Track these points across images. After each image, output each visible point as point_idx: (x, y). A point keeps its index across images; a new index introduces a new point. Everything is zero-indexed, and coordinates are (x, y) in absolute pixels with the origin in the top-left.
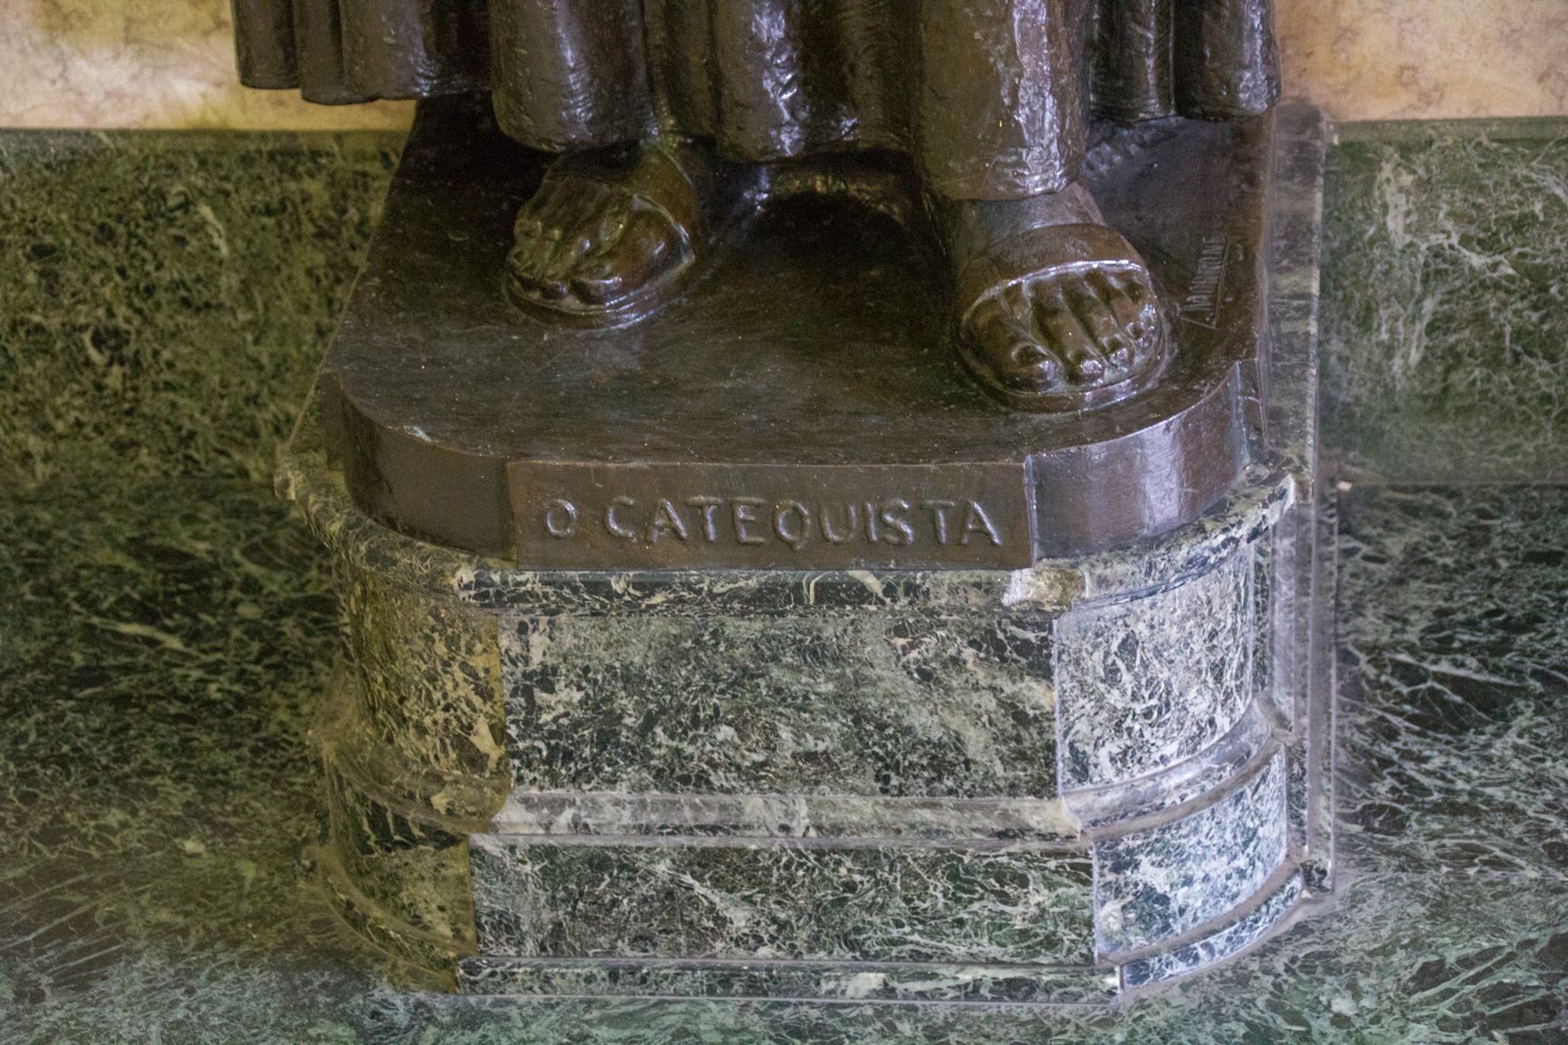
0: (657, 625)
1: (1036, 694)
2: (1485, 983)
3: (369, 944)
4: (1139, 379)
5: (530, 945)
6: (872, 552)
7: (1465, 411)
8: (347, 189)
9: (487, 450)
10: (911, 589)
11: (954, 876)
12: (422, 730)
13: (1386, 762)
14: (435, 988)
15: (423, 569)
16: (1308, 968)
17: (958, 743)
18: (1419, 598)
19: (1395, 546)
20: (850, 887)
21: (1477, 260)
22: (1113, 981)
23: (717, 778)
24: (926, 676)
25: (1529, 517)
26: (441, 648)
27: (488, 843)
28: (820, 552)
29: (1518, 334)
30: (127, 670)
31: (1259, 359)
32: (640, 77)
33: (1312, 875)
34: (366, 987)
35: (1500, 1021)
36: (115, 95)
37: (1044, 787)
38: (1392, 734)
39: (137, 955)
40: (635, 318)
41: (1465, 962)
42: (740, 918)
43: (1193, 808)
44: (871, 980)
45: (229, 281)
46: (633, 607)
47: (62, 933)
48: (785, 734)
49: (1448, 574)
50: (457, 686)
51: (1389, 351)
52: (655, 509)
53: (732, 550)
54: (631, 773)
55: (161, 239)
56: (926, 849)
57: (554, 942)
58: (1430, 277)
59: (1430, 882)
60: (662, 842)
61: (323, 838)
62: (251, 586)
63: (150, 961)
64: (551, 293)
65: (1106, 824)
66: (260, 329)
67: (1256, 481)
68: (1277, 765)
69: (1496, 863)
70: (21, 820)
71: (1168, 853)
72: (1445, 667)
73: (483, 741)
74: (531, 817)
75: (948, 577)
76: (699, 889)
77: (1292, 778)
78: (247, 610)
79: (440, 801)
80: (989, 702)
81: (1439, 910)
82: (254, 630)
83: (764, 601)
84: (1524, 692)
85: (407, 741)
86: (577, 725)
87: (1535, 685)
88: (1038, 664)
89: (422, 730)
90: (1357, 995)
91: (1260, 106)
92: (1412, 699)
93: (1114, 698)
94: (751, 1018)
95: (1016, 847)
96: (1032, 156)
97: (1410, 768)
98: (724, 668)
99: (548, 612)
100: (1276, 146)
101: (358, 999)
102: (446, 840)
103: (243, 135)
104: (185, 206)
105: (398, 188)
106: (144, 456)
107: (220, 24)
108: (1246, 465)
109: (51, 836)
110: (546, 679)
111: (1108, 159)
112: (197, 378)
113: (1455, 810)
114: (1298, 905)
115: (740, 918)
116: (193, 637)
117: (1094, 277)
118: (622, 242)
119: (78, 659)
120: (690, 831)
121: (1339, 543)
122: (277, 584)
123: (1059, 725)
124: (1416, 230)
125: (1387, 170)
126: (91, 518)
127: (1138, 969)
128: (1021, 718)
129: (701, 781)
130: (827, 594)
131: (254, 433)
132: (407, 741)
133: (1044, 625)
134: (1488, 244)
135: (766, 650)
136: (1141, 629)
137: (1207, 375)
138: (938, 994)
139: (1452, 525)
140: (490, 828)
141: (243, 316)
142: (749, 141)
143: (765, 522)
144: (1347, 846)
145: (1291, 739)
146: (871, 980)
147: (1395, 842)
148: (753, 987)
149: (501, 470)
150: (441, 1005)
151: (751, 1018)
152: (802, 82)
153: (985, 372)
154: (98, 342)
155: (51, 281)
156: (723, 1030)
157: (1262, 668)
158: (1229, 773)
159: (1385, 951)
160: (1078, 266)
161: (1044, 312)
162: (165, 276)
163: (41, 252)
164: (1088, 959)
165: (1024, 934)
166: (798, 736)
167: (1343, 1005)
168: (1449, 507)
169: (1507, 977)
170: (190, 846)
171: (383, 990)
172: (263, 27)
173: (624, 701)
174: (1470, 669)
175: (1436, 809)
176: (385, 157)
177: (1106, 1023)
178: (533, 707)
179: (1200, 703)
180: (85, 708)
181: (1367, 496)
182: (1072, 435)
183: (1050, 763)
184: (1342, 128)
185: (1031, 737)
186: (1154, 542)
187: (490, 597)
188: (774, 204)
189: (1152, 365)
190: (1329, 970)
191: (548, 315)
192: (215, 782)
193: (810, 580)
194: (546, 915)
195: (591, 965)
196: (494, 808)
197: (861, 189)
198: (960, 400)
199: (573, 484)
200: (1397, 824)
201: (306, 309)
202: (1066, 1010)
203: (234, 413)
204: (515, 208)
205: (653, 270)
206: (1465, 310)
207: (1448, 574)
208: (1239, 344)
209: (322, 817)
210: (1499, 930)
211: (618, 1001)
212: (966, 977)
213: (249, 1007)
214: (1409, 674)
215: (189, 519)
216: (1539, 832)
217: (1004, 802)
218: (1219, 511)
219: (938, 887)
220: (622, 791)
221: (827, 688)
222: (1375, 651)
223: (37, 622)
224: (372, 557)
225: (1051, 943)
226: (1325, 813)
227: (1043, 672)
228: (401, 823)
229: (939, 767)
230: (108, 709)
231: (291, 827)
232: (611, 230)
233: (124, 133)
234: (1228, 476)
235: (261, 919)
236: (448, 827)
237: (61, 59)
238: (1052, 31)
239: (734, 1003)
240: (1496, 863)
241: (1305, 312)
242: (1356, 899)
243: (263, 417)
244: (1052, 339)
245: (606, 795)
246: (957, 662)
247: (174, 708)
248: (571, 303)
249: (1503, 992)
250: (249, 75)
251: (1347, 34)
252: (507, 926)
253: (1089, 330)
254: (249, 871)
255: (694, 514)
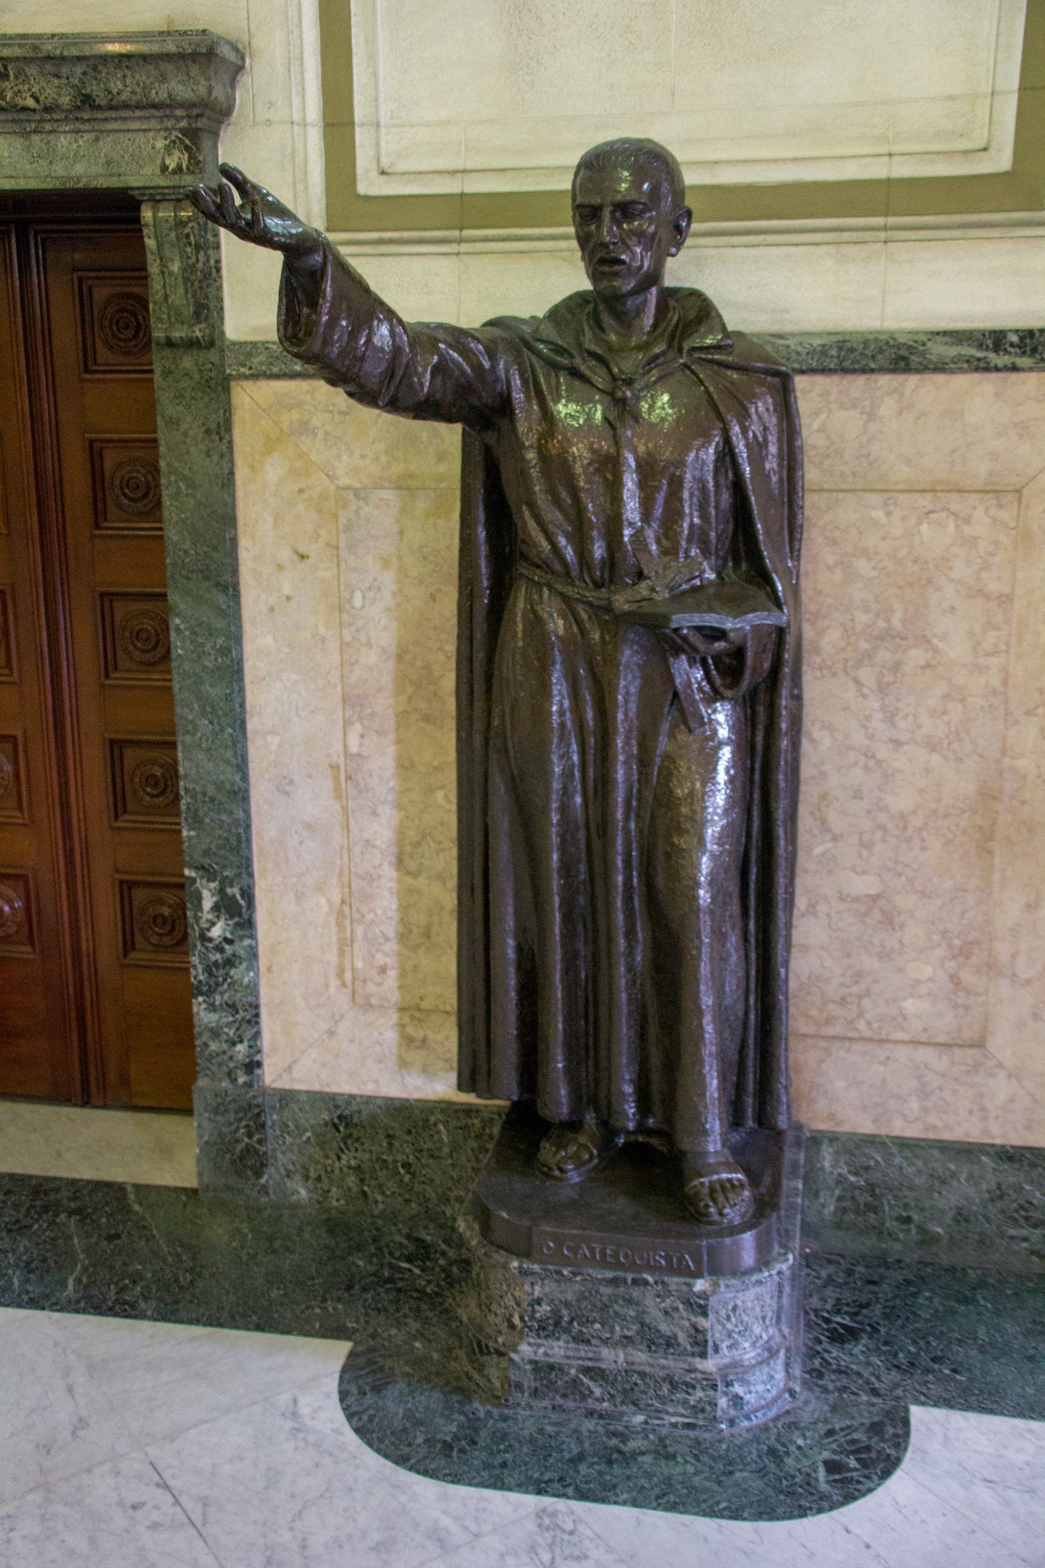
0: (577, 1286)
1: (702, 1322)
2: (849, 1438)
3: (473, 1387)
4: (743, 1216)
5: (526, 1394)
6: (651, 1269)
7: (848, 1229)
8: (488, 1122)
9: (526, 1222)
10: (663, 1283)
11: (671, 1383)
12: (496, 1314)
13: (818, 1352)
14: (494, 1406)
15: (502, 1260)
16: (789, 1427)
17: (675, 1337)
18: (831, 1293)
19: (824, 1273)
20: (636, 1384)
21: (852, 1179)
22: (723, 1426)
23: (594, 1342)
24: (666, 1313)
25: (867, 1267)
26: (505, 1288)
27: (515, 1357)
28: (633, 1267)
29: (866, 1205)
30: (402, 1279)
31: (782, 1212)
32: (585, 1099)
33: (792, 1393)
34: (471, 1402)
35: (853, 1452)
36: (417, 1088)
37: (703, 1355)
38: (820, 1342)
39: (396, 1382)
40: (577, 1180)
41: (842, 1429)
42: (598, 1392)
43: (753, 1366)
44: (640, 1418)
45: (446, 1150)
46: (570, 1280)
47: (374, 1372)
48: (618, 1328)
49: (840, 1286)
50: (509, 1301)
51: (823, 1206)
52: (579, 1247)
53: (604, 1264)
54: (565, 1337)
55: (426, 1135)
56: (662, 1373)
57: (535, 1393)
58: (838, 1182)
59: (832, 1398)
60: (574, 1362)
61: (461, 1347)
62: (443, 1253)
63: (401, 1385)
64: (550, 1169)
65: (724, 1370)
66: (453, 1166)
67: (780, 1254)
68: (782, 1354)
69: (853, 1393)
70: (364, 1330)
71: (744, 1382)
72: (839, 1319)
73: (516, 1320)
74: (530, 1349)
75: (676, 1279)
76: (585, 1380)
77: (788, 1358)
78: (442, 1262)
79: (500, 1340)
80: (687, 1324)
81: (834, 1409)
82: (443, 1270)
83: (614, 1282)
84: (864, 1331)
85: (491, 1318)
86: (548, 1318)
87: (868, 1328)
88: (704, 1312)
89: (496, 1314)
90: (805, 1437)
91: (785, 1127)
92: (828, 1330)
93: (729, 1326)
94: (600, 1428)
95: (693, 1375)
96: (710, 1139)
97: (826, 1356)
98: (599, 1304)
99: (542, 1279)
100: (789, 1137)
101: (468, 1407)
102: (500, 1354)
103: (455, 1103)
104: (435, 1125)
105: (504, 1127)
106: (414, 1205)
107: (452, 1068)
108: (777, 1248)
109: (373, 1336)
110: (539, 1301)
111: (735, 1137)
112: (432, 1180)
113: (840, 1372)
114: (786, 1403)
115: (598, 1392)
116: (423, 1270)
117: (729, 1180)
118: (575, 1154)
119: (386, 1274)
120: (583, 1359)
121: (806, 1271)
122: (452, 1254)
123: (710, 1334)
124: (834, 1167)
125: (824, 1147)
126: (395, 1224)
127: (732, 1422)
128: (697, 1330)
129: (588, 1342)
130: (635, 1282)
131: (449, 1200)
132: (491, 1318)
133: (707, 1299)
134: (856, 1174)
135: (613, 1299)
136: (739, 1303)
137: (764, 1217)
138: (664, 1425)
139: (843, 1267)
140: (516, 1351)
141: (449, 1161)
142: (619, 1125)
143: (616, 1256)
144: (804, 1382)
145: (787, 1344)
146: (640, 1418)
147: (821, 1382)
148: (601, 1416)
149: (530, 1229)
150: (495, 1412)
151: (600, 1428)
152: (637, 1107)
153: (691, 1209)
154: (403, 1166)
155: (390, 1145)
156: (589, 1431)
157: (779, 1318)
158: (766, 1354)
159: (815, 1423)
160: (724, 1176)
161: (712, 1191)
162: (426, 1147)
163: (389, 1136)
164: (715, 1418)
165: (694, 1407)
166: (622, 1329)
167: (800, 1442)
168: (842, 1261)
169: (856, 1436)
170: (417, 1344)
171: (476, 1405)
172: (466, 1074)
173: (565, 1312)
174: (847, 1321)
175: (834, 1371)
176: (500, 1114)
177: (720, 1441)
178: (534, 1311)
179: (757, 1329)
180: (387, 1292)
181: (815, 1254)
182: (720, 1234)
183: (706, 1346)
184: (811, 1131)
185: (700, 1337)
186: (745, 1273)
187: (523, 1272)
188: (625, 1144)
189: (746, 1212)
190: (797, 1428)
191: (548, 1176)
192: (426, 1321)
193: (630, 1277)
194: (533, 1384)
195: (546, 1403)
196: (518, 1344)
197: (654, 1142)
198: (683, 1218)
199: (554, 1237)
200: (821, 1376)
201: (469, 1160)
202: (707, 1435)
203: (444, 1194)
204: (541, 1139)
205: (584, 1164)
206: (849, 1194)
207: (840, 1286)
208: (775, 1207)
209: (461, 1339)
210: (853, 1418)
211: (554, 1417)
212: (673, 1420)
213: (433, 1406)
214: (827, 1321)
215: (426, 1228)
216: (868, 1382)
217: (690, 1359)
218: (767, 1264)
219: (665, 1388)
220: (561, 1343)
221: (632, 1313)
222: (815, 1311)
223: (374, 1260)
224: (485, 1254)
225: (703, 1410)
226: (797, 1371)
227: (705, 1314)
228: (487, 1347)
229: (669, 1345)
230: (394, 1293)
231: (450, 1341)
232: (572, 1149)
233: (419, 1101)
234: (770, 1252)
235: (438, 1374)
236: (502, 1349)
237: (403, 1077)
238: (719, 1099)
239: (594, 1421)
240: (853, 1393)
241: (797, 1195)
242: (806, 1402)
243: (452, 1195)
244: (714, 1200)
245: (555, 1344)
246: (677, 1309)
247: (415, 1295)
248: (557, 1173)
249: (854, 1442)
250: (460, 1087)
251: (812, 1101)
252: (519, 1387)
253: (727, 1198)
254: (435, 1356)
255: (592, 1251)
